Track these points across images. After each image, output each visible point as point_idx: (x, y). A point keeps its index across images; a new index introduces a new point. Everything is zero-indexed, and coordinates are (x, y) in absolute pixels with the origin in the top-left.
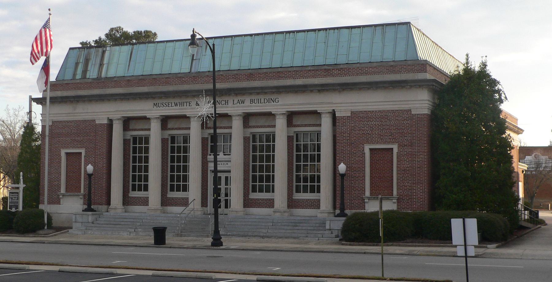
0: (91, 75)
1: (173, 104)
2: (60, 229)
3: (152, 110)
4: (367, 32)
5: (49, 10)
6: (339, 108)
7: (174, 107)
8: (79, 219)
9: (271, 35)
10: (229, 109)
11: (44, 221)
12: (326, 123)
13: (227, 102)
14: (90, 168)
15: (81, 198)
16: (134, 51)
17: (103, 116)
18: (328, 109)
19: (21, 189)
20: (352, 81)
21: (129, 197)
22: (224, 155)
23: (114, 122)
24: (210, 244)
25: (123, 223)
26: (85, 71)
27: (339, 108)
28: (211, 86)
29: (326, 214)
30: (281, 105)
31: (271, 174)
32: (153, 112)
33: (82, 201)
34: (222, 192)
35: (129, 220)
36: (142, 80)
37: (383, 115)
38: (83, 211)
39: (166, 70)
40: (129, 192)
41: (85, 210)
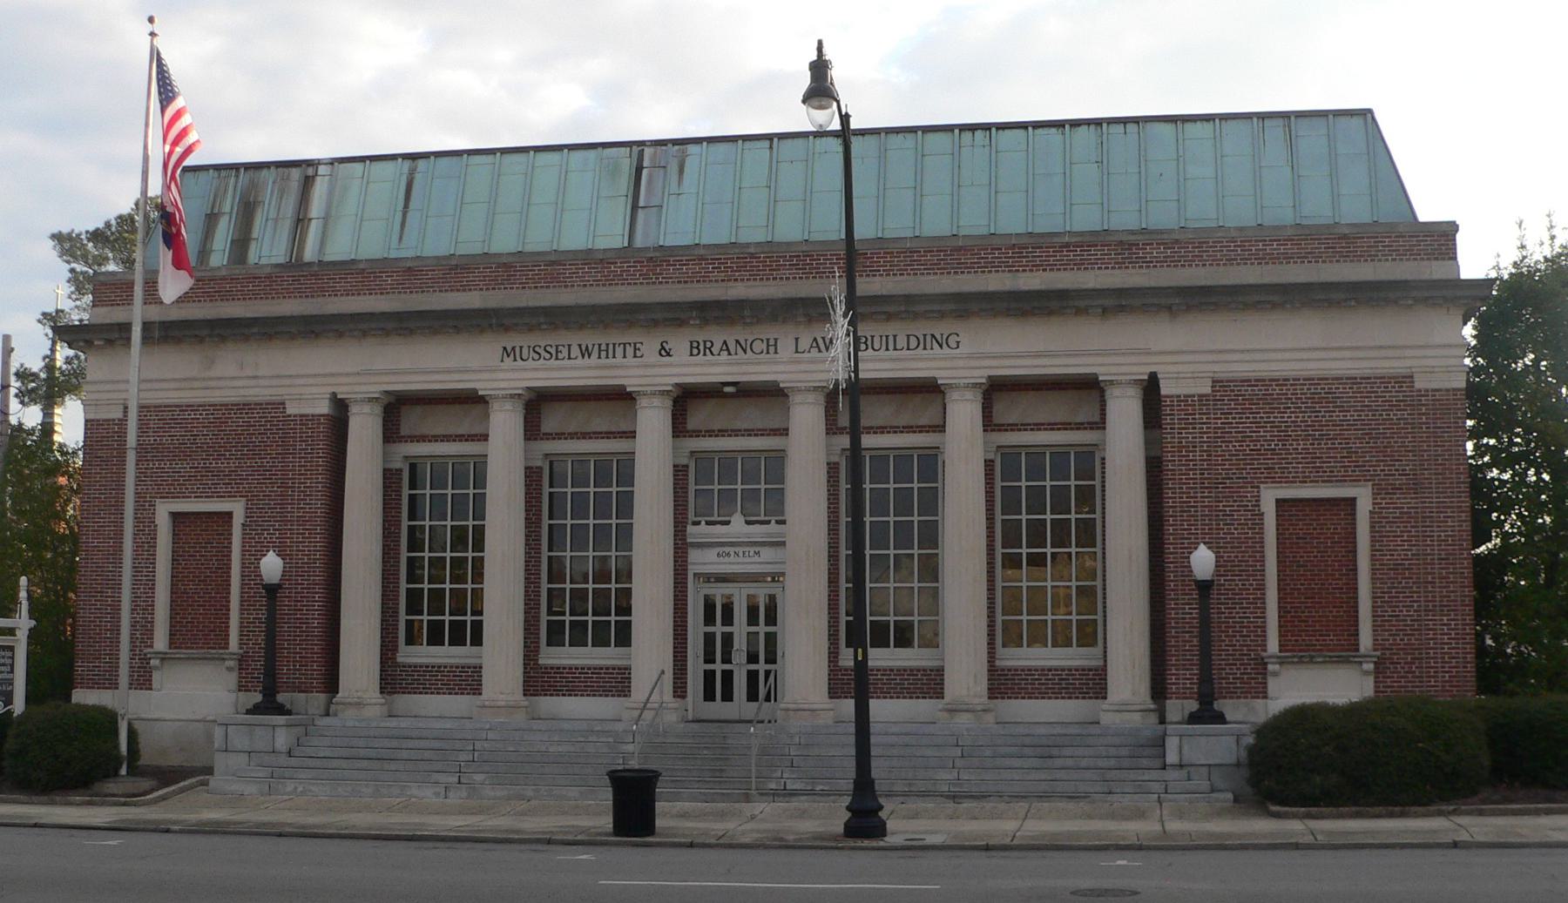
0: (265, 252)
1: (575, 352)
2: (167, 776)
3: (494, 370)
4: (1122, 144)
5: (151, 20)
6: (1171, 368)
7: (580, 361)
8: (239, 739)
9: (910, 136)
10: (781, 368)
11: (117, 746)
12: (1125, 413)
13: (772, 346)
14: (271, 565)
15: (229, 669)
16: (418, 177)
17: (314, 390)
18: (1135, 369)
19: (22, 636)
20: (1302, 279)
21: (397, 665)
22: (748, 523)
23: (354, 409)
24: (841, 829)
25: (404, 754)
26: (241, 244)
27: (1171, 368)
29: (1137, 717)
30: (970, 357)
32: (501, 375)
33: (232, 679)
34: (736, 646)
35: (422, 744)
36: (457, 270)
37: (1321, 393)
38: (248, 712)
39: (539, 239)
40: (395, 649)
41: (256, 710)
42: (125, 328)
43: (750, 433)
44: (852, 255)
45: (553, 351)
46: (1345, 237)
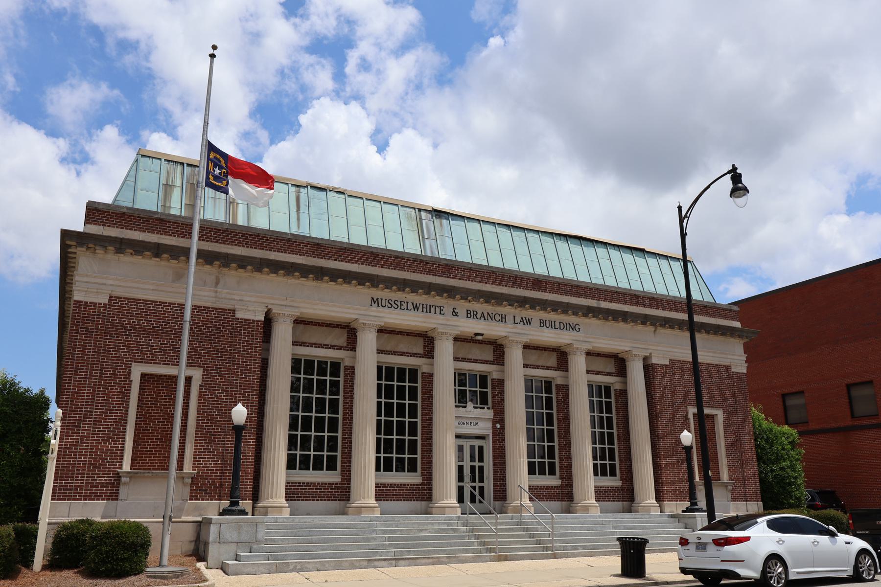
1: (410, 306)
5: (214, 47)
22: (475, 408)
28: (684, 316)
31: (383, 437)
38: (220, 514)
42: (186, 252)
44: (689, 305)
45: (399, 304)
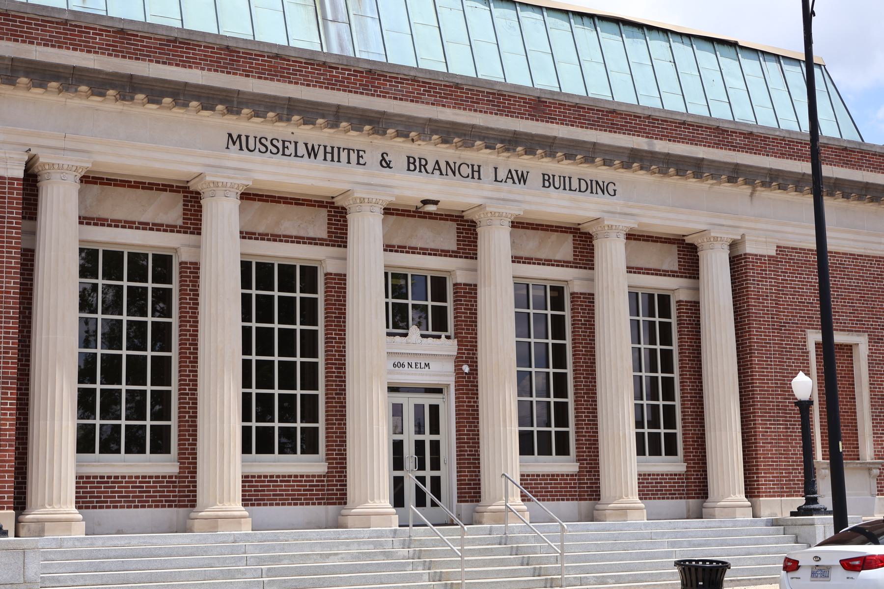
22: (423, 336)
43: (425, 251)
46: (845, 149)
